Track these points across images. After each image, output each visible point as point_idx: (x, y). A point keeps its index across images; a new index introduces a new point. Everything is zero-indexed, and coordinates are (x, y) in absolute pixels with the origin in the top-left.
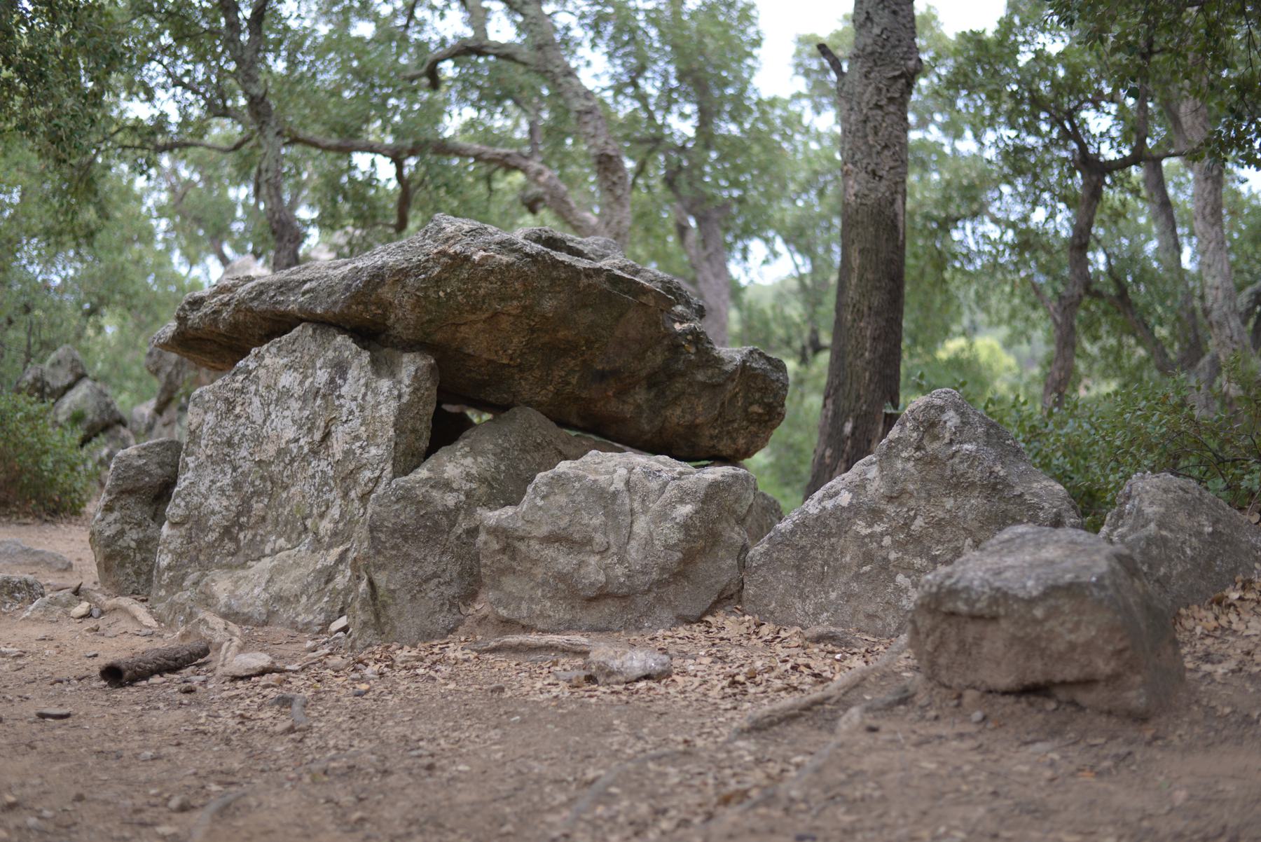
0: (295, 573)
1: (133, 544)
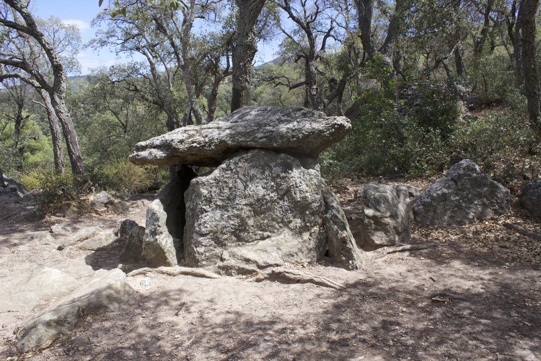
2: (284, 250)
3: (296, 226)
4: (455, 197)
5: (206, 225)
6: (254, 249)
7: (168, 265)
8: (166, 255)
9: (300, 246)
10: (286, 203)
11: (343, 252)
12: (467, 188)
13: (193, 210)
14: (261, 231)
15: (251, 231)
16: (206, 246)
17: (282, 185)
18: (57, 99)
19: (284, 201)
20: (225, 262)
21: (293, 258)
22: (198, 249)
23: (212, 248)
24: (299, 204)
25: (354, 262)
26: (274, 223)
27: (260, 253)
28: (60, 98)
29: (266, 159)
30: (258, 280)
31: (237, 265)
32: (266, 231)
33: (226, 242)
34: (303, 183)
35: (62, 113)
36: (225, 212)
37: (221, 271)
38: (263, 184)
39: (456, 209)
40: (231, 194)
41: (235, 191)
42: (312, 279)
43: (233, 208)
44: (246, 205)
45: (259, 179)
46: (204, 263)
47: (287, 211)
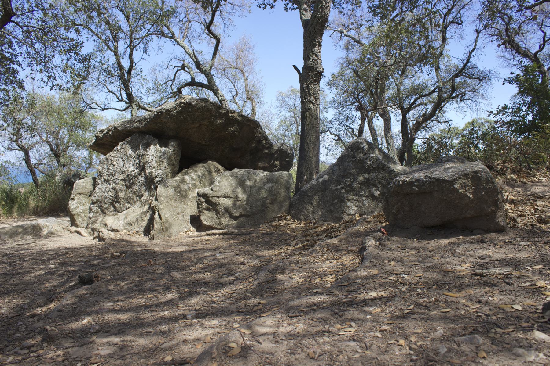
0: (133, 215)
1: (81, 211)
4: (336, 186)
8: (75, 217)
12: (351, 173)
23: (98, 215)
39: (336, 201)
44: (122, 180)
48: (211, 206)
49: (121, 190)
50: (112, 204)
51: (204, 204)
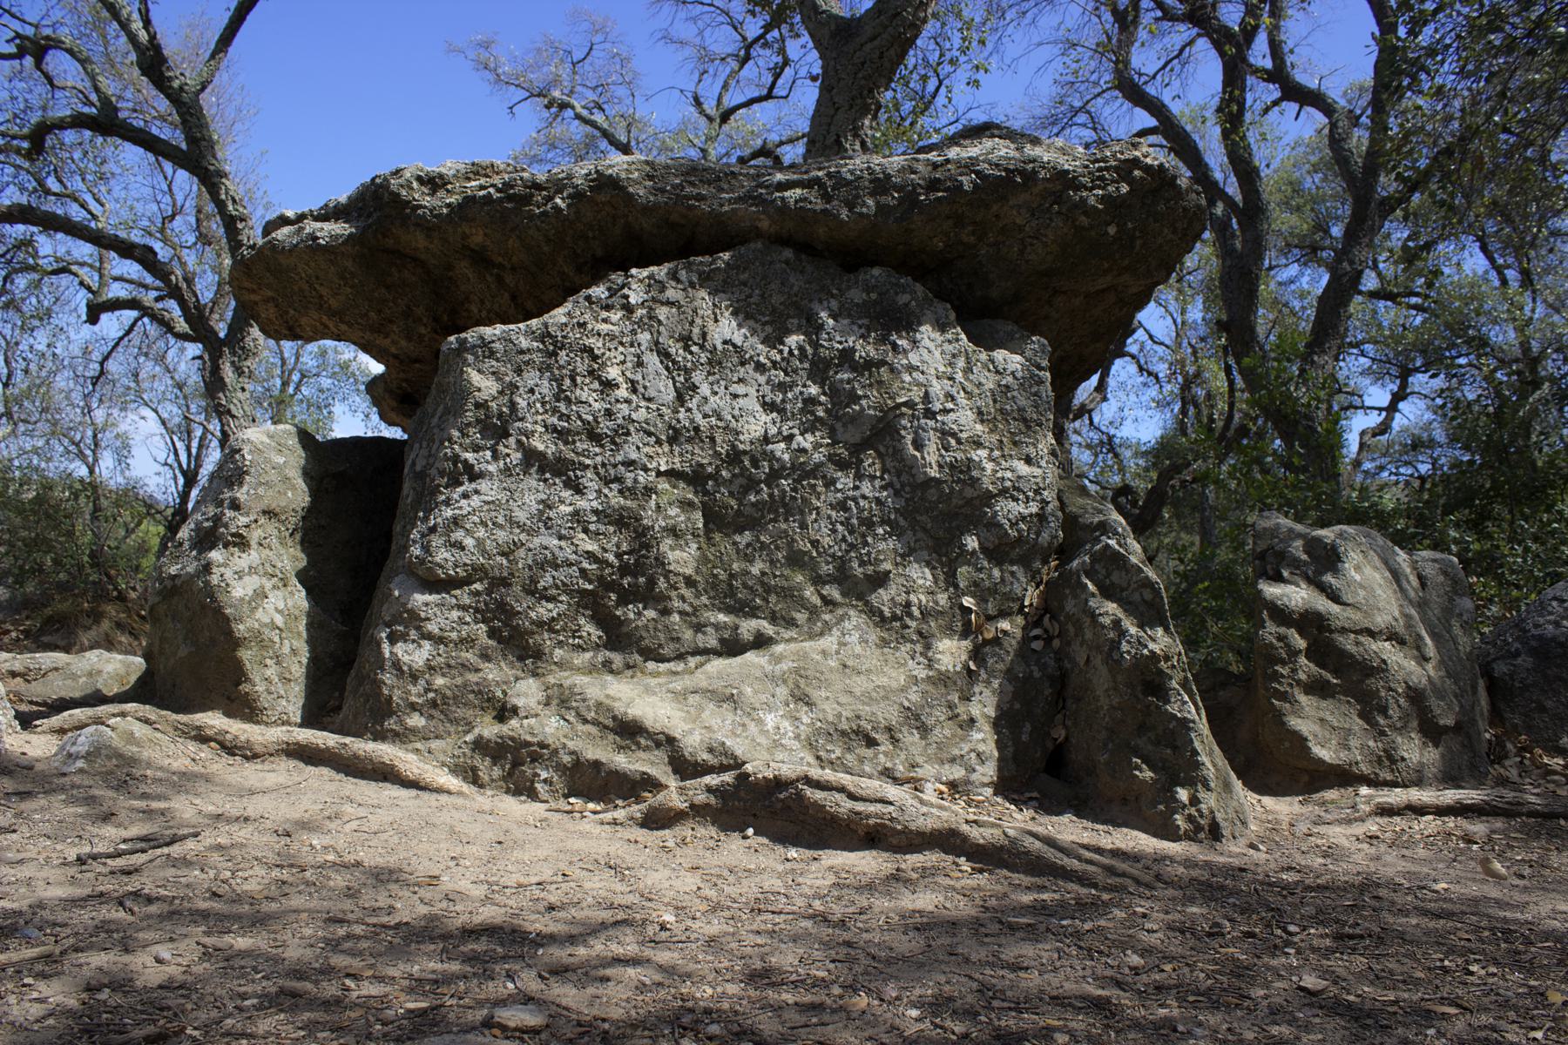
1: (279, 620)
2: (830, 709)
3: (908, 604)
5: (458, 535)
6: (678, 685)
7: (246, 709)
8: (246, 655)
9: (914, 697)
10: (866, 488)
11: (1141, 742)
13: (421, 476)
14: (728, 610)
15: (676, 604)
16: (439, 640)
17: (856, 399)
18: (228, 373)
19: (859, 477)
20: (514, 722)
21: (869, 753)
22: (400, 648)
23: (469, 656)
24: (932, 495)
25: (1202, 795)
26: (799, 578)
27: (701, 709)
28: (239, 371)
29: (796, 282)
30: (657, 820)
31: (571, 745)
32: (753, 613)
33: (546, 640)
34: (961, 398)
35: (233, 417)
36: (566, 494)
37: (484, 766)
38: (767, 389)
40: (609, 413)
41: (628, 401)
42: (953, 833)
43: (607, 482)
44: (672, 474)
45: (750, 368)
46: (416, 721)
47: (869, 523)
48: (1336, 672)
49: (673, 532)
50: (591, 603)
51: (1303, 660)
